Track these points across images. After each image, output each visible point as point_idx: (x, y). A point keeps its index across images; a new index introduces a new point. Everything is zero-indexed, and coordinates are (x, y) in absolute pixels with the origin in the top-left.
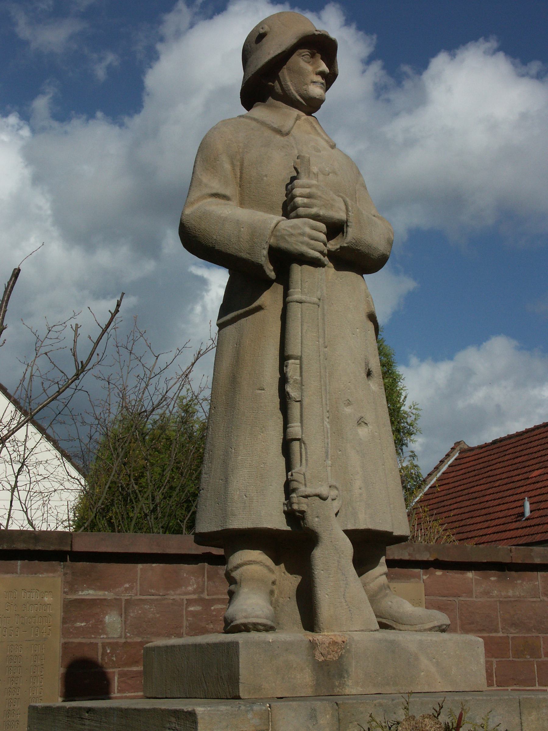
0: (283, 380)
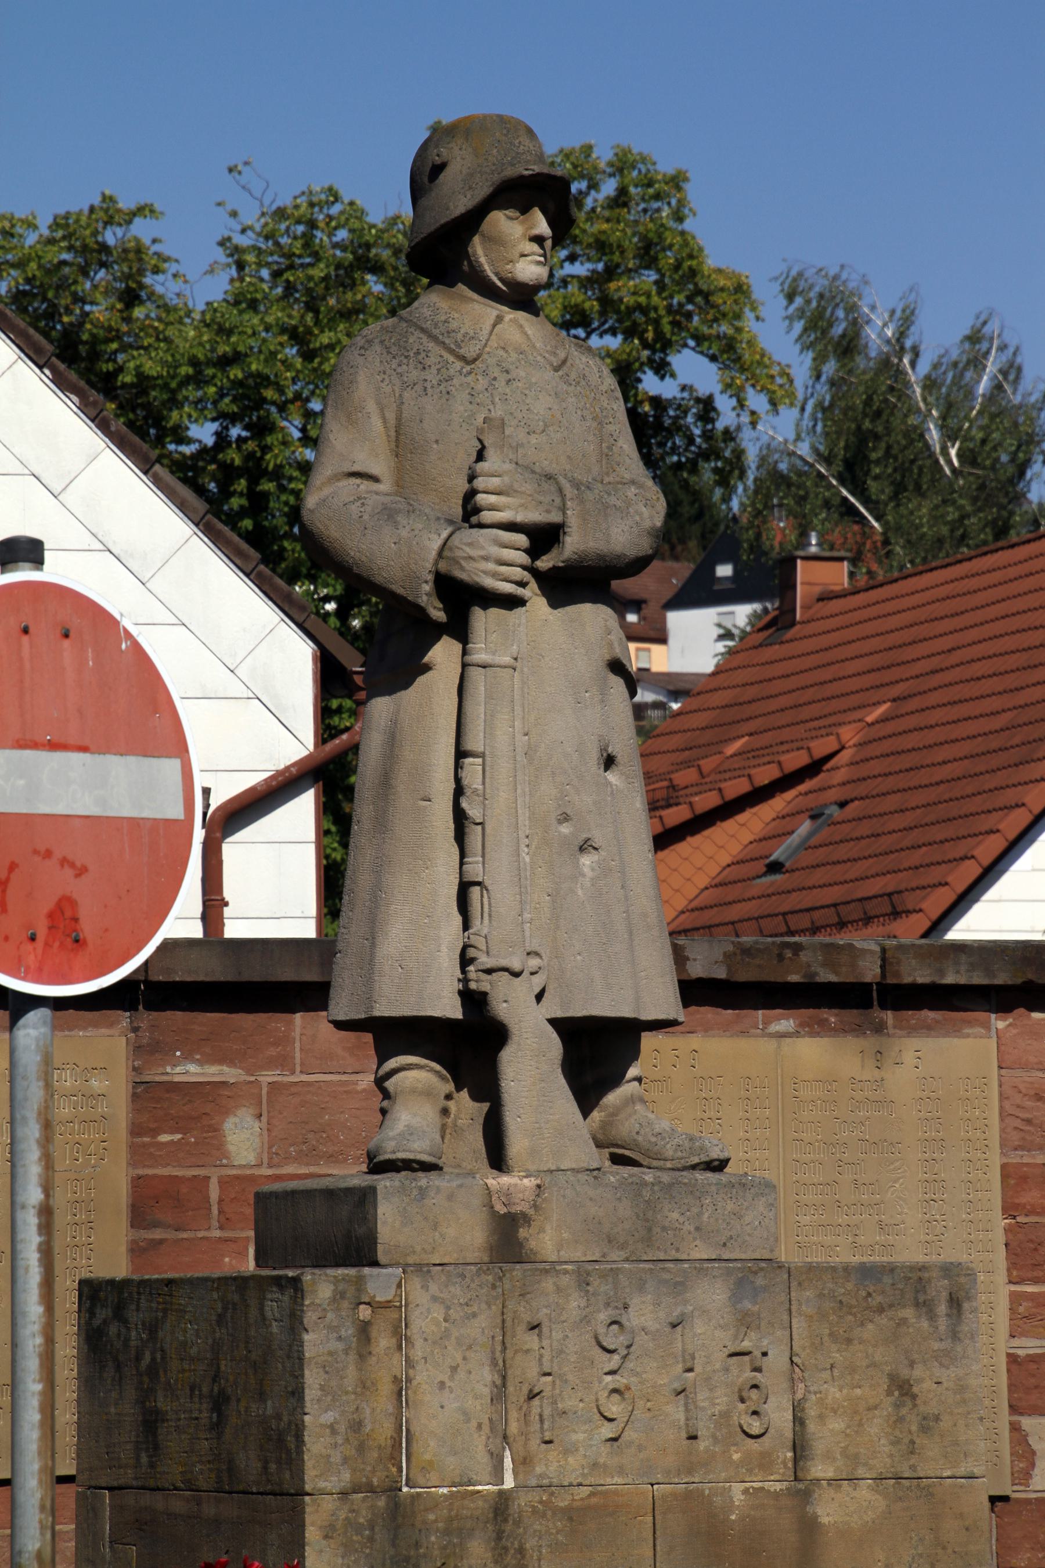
0: (459, 791)
